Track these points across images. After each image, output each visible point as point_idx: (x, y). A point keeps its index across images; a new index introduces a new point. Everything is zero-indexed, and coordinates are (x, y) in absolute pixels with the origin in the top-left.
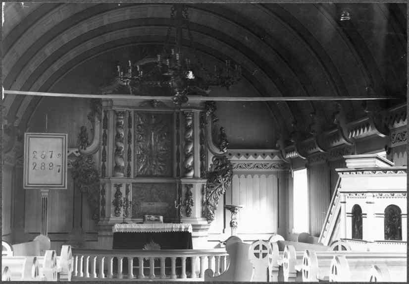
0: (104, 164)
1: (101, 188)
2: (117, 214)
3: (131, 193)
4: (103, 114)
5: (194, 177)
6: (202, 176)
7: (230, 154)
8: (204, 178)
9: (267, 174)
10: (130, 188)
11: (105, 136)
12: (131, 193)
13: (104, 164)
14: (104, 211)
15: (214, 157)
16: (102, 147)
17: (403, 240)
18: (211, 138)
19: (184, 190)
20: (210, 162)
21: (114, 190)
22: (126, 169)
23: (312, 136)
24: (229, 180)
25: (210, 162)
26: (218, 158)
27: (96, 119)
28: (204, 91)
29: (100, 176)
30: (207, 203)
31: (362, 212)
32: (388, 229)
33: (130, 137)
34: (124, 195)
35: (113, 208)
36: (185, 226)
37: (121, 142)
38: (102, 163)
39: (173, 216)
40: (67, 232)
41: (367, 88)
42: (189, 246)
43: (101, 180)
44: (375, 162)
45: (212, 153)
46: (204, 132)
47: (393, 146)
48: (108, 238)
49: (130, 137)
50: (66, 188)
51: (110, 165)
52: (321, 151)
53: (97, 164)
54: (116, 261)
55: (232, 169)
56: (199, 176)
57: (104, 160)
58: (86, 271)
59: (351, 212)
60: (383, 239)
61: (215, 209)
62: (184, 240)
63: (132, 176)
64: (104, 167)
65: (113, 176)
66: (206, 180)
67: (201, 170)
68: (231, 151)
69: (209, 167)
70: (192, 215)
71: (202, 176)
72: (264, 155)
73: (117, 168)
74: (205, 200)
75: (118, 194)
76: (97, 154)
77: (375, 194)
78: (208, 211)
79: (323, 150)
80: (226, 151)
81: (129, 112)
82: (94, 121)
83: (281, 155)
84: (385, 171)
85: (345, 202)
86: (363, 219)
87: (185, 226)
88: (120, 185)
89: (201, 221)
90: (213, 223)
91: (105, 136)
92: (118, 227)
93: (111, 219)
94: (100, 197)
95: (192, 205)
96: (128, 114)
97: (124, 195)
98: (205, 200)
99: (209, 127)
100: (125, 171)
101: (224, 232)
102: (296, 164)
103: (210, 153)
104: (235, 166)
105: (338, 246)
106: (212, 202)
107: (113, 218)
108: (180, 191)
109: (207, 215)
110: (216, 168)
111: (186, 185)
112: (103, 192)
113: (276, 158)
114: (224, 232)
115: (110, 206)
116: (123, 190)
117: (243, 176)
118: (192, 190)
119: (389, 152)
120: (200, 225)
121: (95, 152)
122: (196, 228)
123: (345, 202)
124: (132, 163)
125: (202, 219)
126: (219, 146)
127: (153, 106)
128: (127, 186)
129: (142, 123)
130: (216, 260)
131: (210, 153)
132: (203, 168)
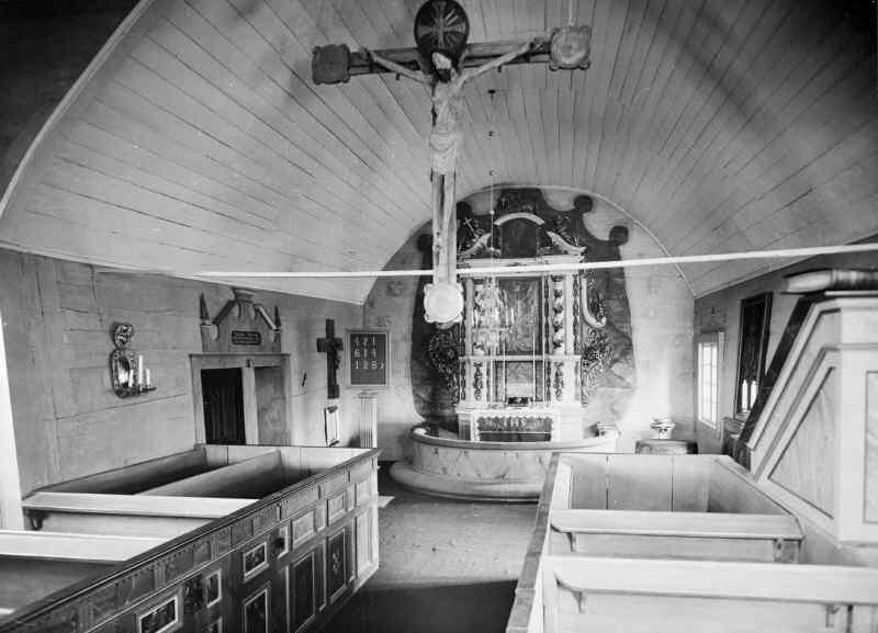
21: (474, 370)
43: (460, 358)
116: (483, 370)
128: (489, 364)
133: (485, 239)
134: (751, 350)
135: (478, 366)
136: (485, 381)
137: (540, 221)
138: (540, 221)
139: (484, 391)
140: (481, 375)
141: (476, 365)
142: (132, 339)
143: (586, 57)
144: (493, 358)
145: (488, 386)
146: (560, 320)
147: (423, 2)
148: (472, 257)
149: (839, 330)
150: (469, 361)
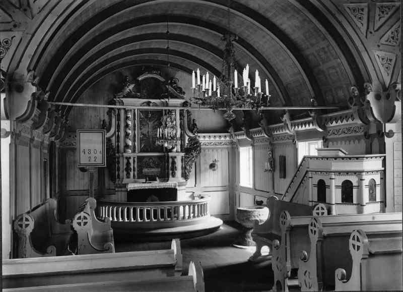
0: (118, 144)
1: (117, 160)
2: (128, 177)
3: (136, 163)
4: (117, 111)
5: (177, 152)
6: (182, 151)
7: (199, 137)
8: (183, 152)
9: (222, 149)
10: (136, 159)
11: (118, 126)
12: (136, 163)
13: (118, 144)
14: (119, 175)
15: (189, 139)
16: (117, 133)
17: (354, 203)
18: (187, 127)
19: (170, 160)
20: (187, 142)
21: (125, 161)
22: (133, 147)
23: (260, 126)
24: (199, 153)
25: (187, 142)
26: (191, 139)
27: (113, 115)
28: (183, 95)
29: (116, 152)
30: (185, 168)
31: (325, 183)
32: (344, 196)
33: (134, 126)
34: (132, 164)
35: (125, 173)
36: (171, 183)
37: (129, 129)
38: (117, 144)
39: (165, 177)
40: (359, 264)
41: (312, 100)
42: (175, 198)
43: (117, 154)
44: (338, 153)
45: (188, 136)
46: (182, 123)
47: (328, 137)
48: (123, 193)
49: (134, 126)
50: (106, 166)
51: (122, 145)
52: (266, 136)
53: (114, 145)
54: (135, 210)
55: (200, 146)
56: (180, 151)
57: (118, 141)
58: (125, 217)
59: (316, 184)
60: (341, 202)
61: (190, 172)
62: (171, 194)
63: (137, 152)
64: (118, 146)
65: (124, 152)
66: (184, 154)
67: (181, 147)
68: (199, 134)
69: (186, 145)
70: (176, 176)
71: (182, 151)
72: (220, 136)
73: (127, 146)
74: (184, 166)
75: (128, 164)
76: (114, 138)
77: (336, 173)
78: (185, 173)
79: (268, 136)
80: (196, 135)
81: (134, 110)
82: (111, 116)
83: (231, 136)
84: (343, 158)
85: (312, 178)
86: (327, 189)
87: (171, 183)
88: (130, 158)
89: (182, 180)
90: (189, 181)
91: (118, 126)
92: (131, 186)
93: (124, 180)
94: (116, 165)
95: (176, 170)
96: (133, 110)
97: (132, 164)
98: (184, 166)
99: (186, 119)
100: (132, 148)
101: (195, 186)
102: (242, 143)
103: (186, 136)
104: (202, 144)
105: (324, 209)
106: (188, 167)
107: (125, 181)
108: (168, 162)
109: (185, 176)
110: (190, 146)
111: (172, 157)
112: (119, 162)
113: (228, 138)
114: (195, 186)
115: (123, 172)
116: (131, 161)
117: (211, 150)
118: (176, 160)
119: (326, 141)
120: (182, 183)
121: (112, 136)
122: (180, 185)
123: (312, 178)
124: (136, 144)
125: (182, 178)
126: (191, 131)
127: (149, 105)
128: (134, 158)
129: (142, 117)
130: (198, 207)
131: (186, 136)
132: (182, 146)
133: (131, 87)
134: (382, 81)
135: (128, 158)
136: (132, 167)
137: (162, 79)
138: (162, 79)
139: (132, 173)
140: (130, 164)
141: (127, 158)
142: (235, 53)
143: (103, 245)
144: (137, 154)
145: (134, 171)
146: (246, 155)
147: (269, 291)
148: (124, 97)
149: (4, 119)
150: (123, 156)
